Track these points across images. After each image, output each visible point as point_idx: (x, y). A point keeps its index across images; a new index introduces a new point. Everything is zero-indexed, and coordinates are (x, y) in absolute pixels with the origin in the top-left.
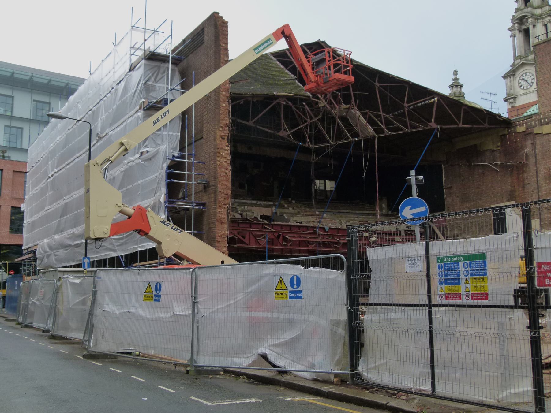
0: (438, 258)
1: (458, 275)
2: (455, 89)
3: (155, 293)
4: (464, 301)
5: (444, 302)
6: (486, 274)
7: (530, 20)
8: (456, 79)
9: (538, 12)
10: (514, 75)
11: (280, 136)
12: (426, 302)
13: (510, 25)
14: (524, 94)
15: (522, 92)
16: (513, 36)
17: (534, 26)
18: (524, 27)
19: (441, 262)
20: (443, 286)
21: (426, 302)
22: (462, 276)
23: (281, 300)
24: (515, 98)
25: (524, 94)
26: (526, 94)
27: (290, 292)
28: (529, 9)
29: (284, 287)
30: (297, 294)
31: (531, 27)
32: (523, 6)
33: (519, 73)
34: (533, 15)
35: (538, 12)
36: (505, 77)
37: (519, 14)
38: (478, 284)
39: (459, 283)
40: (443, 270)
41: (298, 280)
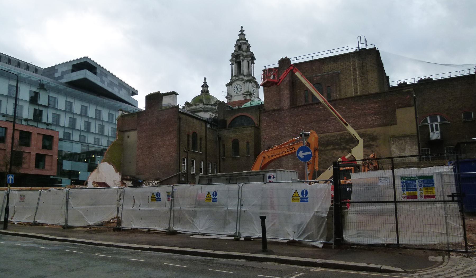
0: (401, 178)
1: (415, 186)
3: (157, 197)
4: (419, 199)
5: (406, 200)
6: (433, 185)
7: (241, 57)
9: (245, 54)
10: (232, 85)
11: (235, 102)
12: (393, 200)
13: (231, 58)
14: (236, 96)
15: (236, 94)
16: (232, 64)
17: (243, 61)
18: (238, 61)
19: (404, 179)
20: (405, 192)
21: (393, 200)
22: (418, 187)
23: (295, 202)
24: (232, 97)
25: (236, 96)
26: (237, 96)
27: (301, 198)
28: (241, 52)
29: (297, 196)
30: (305, 200)
31: (242, 61)
32: (238, 50)
33: (234, 84)
34: (243, 55)
35: (245, 54)
36: (227, 85)
37: (236, 54)
38: (429, 191)
39: (416, 190)
40: (405, 184)
41: (159, 194)
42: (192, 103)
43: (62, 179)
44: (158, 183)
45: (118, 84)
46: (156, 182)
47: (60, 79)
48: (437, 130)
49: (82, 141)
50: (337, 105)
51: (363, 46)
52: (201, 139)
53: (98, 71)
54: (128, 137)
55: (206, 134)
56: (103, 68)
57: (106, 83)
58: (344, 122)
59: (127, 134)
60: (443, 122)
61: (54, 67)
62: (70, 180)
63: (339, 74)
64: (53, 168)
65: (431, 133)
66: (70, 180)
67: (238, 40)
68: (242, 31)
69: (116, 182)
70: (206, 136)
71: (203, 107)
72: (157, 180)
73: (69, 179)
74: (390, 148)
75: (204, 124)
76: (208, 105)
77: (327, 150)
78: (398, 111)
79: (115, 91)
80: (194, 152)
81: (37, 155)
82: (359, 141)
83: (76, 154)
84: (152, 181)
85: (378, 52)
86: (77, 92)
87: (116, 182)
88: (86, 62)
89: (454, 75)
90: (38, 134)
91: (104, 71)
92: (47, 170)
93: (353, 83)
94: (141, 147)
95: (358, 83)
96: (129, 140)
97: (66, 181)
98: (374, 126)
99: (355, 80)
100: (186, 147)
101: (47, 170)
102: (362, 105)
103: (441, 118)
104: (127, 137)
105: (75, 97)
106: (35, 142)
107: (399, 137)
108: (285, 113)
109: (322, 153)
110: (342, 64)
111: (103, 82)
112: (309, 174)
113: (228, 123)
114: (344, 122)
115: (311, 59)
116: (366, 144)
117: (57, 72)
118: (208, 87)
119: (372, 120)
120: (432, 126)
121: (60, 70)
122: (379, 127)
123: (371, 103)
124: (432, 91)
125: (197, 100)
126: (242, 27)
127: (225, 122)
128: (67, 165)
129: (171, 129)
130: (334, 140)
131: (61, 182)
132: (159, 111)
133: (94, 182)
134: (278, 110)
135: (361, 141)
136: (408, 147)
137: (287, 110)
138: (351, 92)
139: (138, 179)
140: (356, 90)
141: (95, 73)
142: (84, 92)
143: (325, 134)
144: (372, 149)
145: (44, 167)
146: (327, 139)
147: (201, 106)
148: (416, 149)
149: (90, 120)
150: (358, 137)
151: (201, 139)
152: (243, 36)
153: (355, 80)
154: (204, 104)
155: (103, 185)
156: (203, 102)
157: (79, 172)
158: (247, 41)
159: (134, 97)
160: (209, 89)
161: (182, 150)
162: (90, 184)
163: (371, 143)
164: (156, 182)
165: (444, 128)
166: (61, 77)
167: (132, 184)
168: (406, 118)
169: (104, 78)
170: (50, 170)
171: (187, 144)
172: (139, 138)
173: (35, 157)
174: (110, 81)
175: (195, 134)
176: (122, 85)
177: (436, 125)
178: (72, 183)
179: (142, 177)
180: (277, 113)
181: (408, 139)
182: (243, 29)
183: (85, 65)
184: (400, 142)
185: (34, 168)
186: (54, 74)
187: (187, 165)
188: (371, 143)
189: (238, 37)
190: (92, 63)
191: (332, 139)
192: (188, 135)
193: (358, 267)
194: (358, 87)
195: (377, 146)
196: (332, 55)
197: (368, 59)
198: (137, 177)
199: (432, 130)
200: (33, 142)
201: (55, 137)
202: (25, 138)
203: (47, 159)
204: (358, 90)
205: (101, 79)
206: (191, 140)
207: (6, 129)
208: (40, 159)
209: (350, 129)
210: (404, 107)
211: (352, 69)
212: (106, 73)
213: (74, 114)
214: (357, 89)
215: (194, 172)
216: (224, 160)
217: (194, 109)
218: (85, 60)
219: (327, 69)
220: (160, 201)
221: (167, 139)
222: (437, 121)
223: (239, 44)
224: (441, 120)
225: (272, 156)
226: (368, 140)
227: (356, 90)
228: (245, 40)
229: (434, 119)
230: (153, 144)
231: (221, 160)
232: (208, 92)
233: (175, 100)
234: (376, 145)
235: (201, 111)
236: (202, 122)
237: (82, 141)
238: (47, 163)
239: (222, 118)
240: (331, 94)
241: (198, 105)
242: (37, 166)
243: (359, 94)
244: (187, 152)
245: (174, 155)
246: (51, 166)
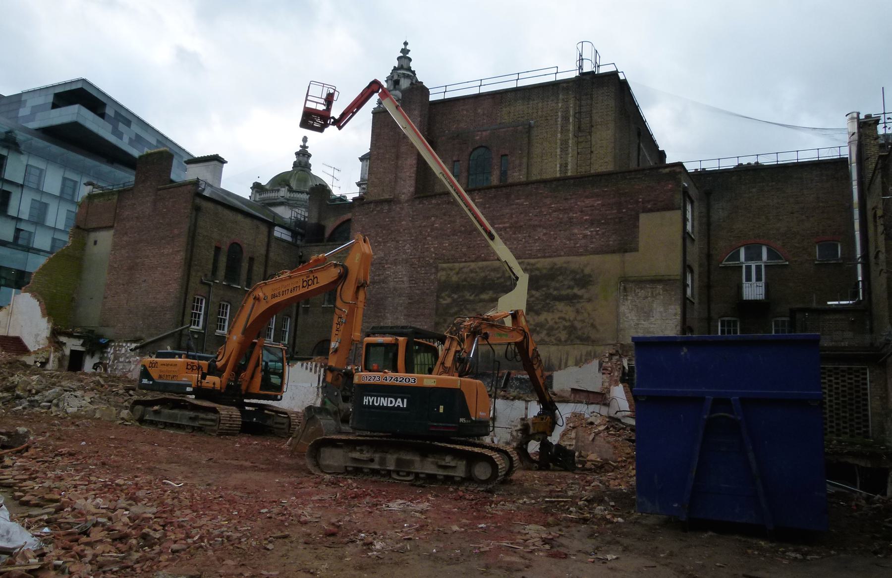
2: (301, 158)
8: (304, 147)
42: (268, 187)
44: (136, 348)
46: (134, 345)
47: (28, 122)
48: (759, 279)
50: (513, 196)
51: (587, 68)
52: (251, 259)
53: (109, 111)
54: (95, 243)
55: (268, 251)
56: (121, 107)
57: (126, 139)
58: (486, 230)
59: (93, 236)
60: (773, 262)
63: (530, 127)
65: (746, 285)
67: (395, 69)
68: (405, 51)
70: (267, 256)
71: (288, 195)
72: (135, 341)
74: (618, 307)
75: (264, 229)
76: (299, 192)
77: (481, 301)
78: (644, 218)
80: (229, 287)
82: (517, 278)
84: (127, 342)
85: (624, 86)
86: (55, 149)
89: (806, 156)
93: (558, 150)
94: (116, 266)
95: (570, 150)
96: (95, 249)
98: (587, 252)
99: (564, 143)
100: (210, 274)
102: (566, 199)
103: (769, 251)
105: (50, 159)
107: (641, 282)
108: (402, 209)
109: (468, 306)
110: (540, 105)
111: (120, 136)
112: (336, 351)
113: (328, 233)
114: (486, 230)
115: (475, 91)
118: (309, 156)
119: (585, 236)
120: (749, 268)
121: (31, 102)
122: (598, 254)
123: (587, 197)
124: (754, 190)
125: (281, 180)
126: (406, 44)
127: (319, 229)
129: (176, 231)
130: (498, 278)
132: (160, 189)
134: (389, 201)
135: (524, 280)
136: (658, 308)
137: (407, 201)
138: (553, 170)
139: (101, 337)
140: (564, 166)
141: (102, 115)
142: (72, 150)
143: (481, 264)
144: (579, 306)
146: (482, 275)
147: (283, 192)
148: (675, 314)
150: (518, 270)
151: (251, 259)
152: (406, 61)
153: (564, 143)
154: (291, 190)
156: (289, 185)
158: (414, 72)
160: (311, 161)
161: (194, 282)
163: (576, 291)
164: (134, 345)
165: (774, 277)
167: (82, 345)
168: (661, 238)
169: (121, 127)
171: (210, 267)
172: (115, 246)
174: (137, 135)
175: (235, 250)
177: (758, 268)
179: (109, 332)
180: (386, 207)
181: (660, 287)
182: (408, 47)
183: (80, 94)
184: (642, 293)
186: (18, 109)
187: (206, 314)
188: (576, 291)
189: (396, 64)
190: (68, 88)
191: (493, 275)
192: (218, 249)
194: (569, 160)
195: (589, 300)
196: (521, 84)
197: (603, 96)
198: (101, 331)
199: (749, 279)
204: (569, 167)
206: (223, 260)
209: (501, 250)
210: (658, 210)
211: (559, 119)
212: (124, 117)
213: (43, 193)
214: (566, 164)
215: (200, 327)
216: (306, 310)
217: (270, 199)
218: (79, 86)
219: (507, 115)
221: (166, 251)
222: (759, 257)
223: (396, 77)
224: (769, 257)
225: (274, 296)
226: (572, 283)
227: (564, 166)
228: (409, 69)
229: (754, 255)
230: (138, 260)
231: (301, 310)
232: (308, 166)
233: (218, 175)
234: (586, 296)
235: (281, 204)
236: (258, 223)
239: (314, 221)
240: (509, 172)
241: (278, 190)
243: (569, 174)
244: (209, 285)
245: (174, 288)
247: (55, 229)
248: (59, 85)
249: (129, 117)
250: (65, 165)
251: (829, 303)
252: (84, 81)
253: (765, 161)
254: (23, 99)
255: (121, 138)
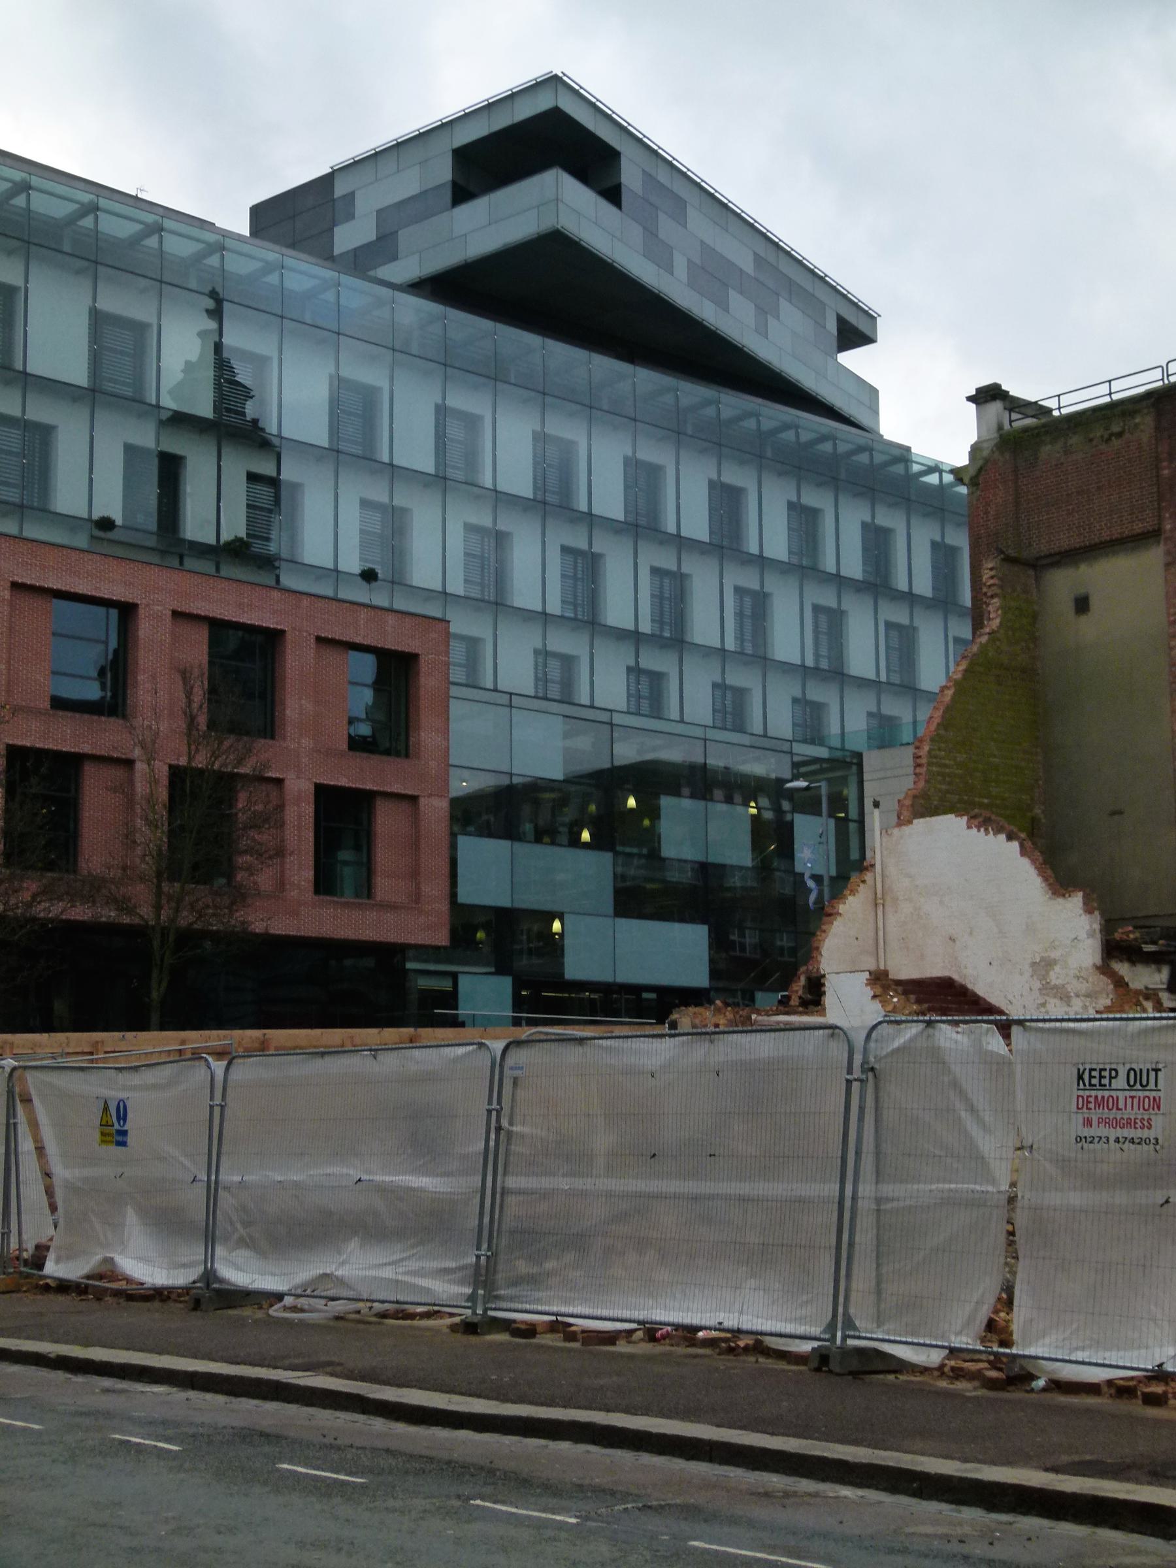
3: (117, 1126)
43: (454, 976)
45: (748, 266)
49: (557, 687)
53: (630, 176)
54: (1082, 605)
59: (1062, 583)
61: (324, 183)
62: (505, 984)
64: (425, 889)
66: (505, 984)
69: (1056, 976)
73: (500, 971)
79: (735, 321)
81: (323, 793)
83: (534, 789)
87: (1056, 976)
88: (556, 116)
90: (319, 640)
91: (663, 176)
92: (393, 907)
96: (1088, 628)
97: (485, 991)
101: (393, 907)
104: (1068, 607)
106: (308, 706)
111: (661, 255)
116: (620, 885)
117: (350, 216)
121: (372, 199)
128: (492, 872)
131: (450, 998)
133: (880, 980)
141: (613, 195)
145: (366, 889)
149: (602, 544)
155: (946, 998)
157: (551, 916)
159: (851, 359)
162: (849, 1001)
166: (383, 247)
170: (399, 914)
173: (309, 809)
176: (783, 273)
178: (518, 1003)
185: (309, 895)
190: (501, 121)
193: (259, 1382)
200: (295, 705)
201: (424, 666)
202: (245, 666)
203: (387, 822)
205: (651, 233)
207: (127, 611)
208: (344, 818)
218: (542, 103)
220: (123, 1144)
237: (557, 687)
238: (385, 856)
242: (325, 883)
246: (415, 874)
247: (544, 617)
248: (467, 117)
249: (679, 188)
250: (543, 393)
251: (573, 1520)
252: (554, 81)
253: (1126, 389)
254: (339, 191)
255: (670, 269)
